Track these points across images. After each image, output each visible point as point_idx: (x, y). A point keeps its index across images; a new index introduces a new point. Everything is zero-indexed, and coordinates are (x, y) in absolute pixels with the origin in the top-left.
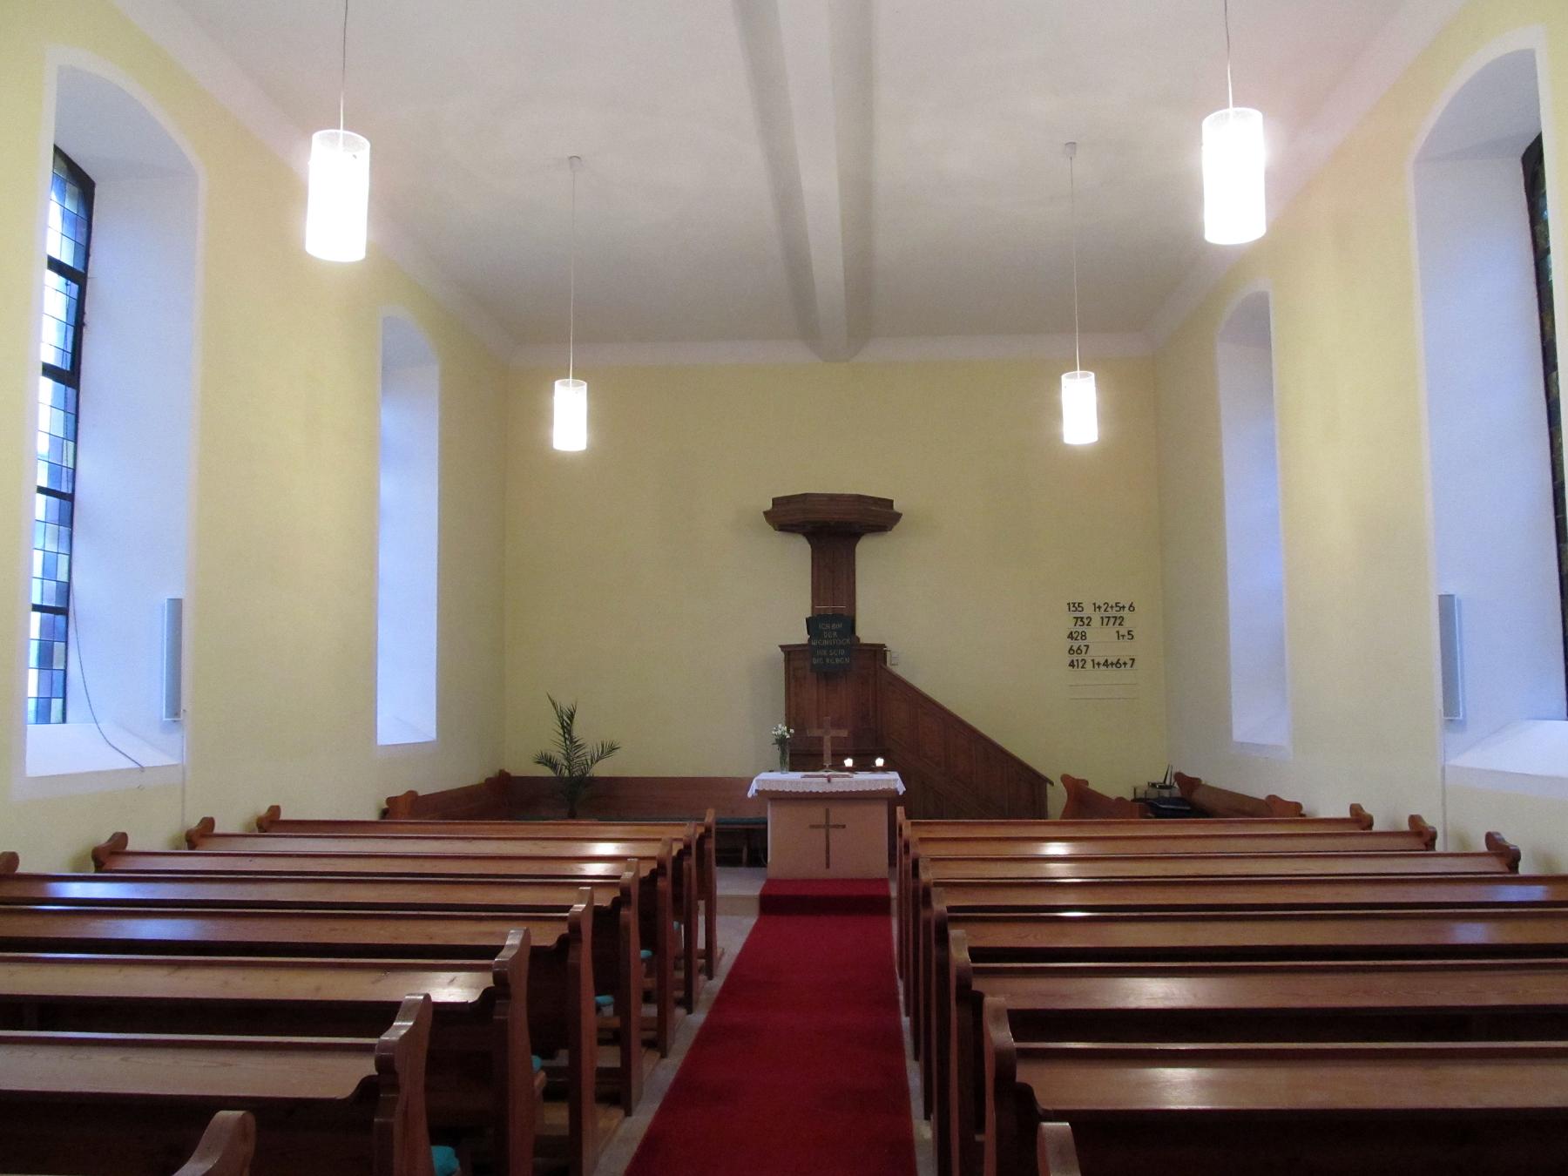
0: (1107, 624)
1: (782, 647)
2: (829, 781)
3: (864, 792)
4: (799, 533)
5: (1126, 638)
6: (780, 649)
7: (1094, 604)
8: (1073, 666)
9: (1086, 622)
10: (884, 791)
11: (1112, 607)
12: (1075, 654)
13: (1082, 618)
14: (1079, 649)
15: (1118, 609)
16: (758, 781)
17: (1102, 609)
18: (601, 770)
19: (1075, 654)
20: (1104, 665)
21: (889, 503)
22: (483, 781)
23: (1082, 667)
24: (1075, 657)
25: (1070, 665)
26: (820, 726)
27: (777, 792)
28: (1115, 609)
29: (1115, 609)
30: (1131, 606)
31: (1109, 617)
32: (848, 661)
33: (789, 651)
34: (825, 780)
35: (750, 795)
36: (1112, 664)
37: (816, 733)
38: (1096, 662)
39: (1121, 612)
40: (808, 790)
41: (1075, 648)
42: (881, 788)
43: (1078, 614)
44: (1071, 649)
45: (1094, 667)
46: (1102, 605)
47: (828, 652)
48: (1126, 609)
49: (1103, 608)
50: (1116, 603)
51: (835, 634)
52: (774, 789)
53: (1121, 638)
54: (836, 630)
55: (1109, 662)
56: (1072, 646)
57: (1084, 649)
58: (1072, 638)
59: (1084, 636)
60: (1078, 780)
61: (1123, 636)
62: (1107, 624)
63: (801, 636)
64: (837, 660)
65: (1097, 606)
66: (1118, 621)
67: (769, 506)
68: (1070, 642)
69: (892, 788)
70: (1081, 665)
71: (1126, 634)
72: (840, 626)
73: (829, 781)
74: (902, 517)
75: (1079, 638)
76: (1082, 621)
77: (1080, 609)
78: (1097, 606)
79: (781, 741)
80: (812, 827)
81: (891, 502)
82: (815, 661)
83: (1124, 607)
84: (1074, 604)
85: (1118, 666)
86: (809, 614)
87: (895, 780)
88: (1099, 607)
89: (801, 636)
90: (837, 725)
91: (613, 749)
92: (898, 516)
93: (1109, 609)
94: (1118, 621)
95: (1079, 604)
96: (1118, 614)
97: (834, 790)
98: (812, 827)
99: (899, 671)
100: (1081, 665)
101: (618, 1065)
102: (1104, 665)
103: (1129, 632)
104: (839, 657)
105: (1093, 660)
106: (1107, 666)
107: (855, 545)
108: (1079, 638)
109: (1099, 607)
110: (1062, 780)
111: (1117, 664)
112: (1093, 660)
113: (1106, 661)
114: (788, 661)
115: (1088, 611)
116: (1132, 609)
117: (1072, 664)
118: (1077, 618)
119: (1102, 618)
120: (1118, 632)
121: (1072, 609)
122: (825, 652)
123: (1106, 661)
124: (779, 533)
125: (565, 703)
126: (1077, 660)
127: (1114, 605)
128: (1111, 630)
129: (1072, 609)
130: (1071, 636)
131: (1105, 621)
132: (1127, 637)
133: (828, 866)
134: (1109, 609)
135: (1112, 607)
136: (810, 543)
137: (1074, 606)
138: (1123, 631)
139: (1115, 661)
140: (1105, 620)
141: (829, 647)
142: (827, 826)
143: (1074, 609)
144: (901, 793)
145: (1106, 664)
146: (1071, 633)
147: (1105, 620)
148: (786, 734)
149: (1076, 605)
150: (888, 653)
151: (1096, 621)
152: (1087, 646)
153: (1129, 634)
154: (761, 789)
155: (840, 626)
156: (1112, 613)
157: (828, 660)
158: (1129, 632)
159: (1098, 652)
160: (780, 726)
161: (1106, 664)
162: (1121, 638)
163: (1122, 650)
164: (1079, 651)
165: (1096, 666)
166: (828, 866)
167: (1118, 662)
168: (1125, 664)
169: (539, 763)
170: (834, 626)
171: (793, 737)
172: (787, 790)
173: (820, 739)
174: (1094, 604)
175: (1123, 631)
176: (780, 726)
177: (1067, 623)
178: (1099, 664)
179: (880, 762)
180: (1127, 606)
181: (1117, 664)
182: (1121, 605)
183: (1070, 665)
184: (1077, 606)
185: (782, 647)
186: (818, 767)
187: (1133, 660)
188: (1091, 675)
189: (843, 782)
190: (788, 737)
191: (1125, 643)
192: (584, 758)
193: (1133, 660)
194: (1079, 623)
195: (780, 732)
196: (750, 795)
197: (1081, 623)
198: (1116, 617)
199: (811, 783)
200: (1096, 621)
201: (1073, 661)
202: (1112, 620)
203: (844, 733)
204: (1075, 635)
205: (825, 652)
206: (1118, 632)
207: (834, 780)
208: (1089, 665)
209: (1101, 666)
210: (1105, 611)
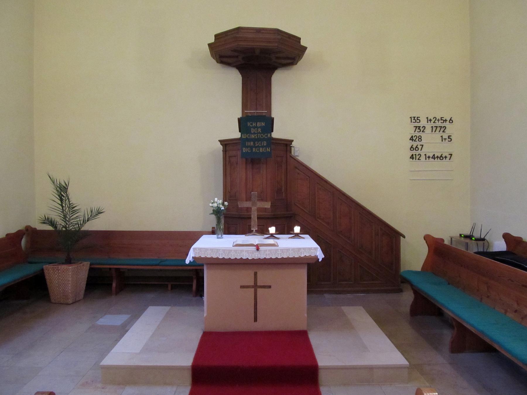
0: (435, 132)
1: (221, 141)
2: (258, 249)
3: (288, 259)
4: (234, 66)
5: (447, 141)
6: (219, 143)
7: (427, 118)
8: (413, 158)
9: (422, 130)
10: (305, 258)
11: (438, 120)
12: (414, 151)
13: (420, 127)
14: (416, 147)
15: (442, 121)
16: (194, 249)
17: (432, 122)
18: (87, 227)
19: (414, 151)
20: (432, 158)
21: (298, 39)
22: (4, 236)
23: (418, 159)
24: (414, 152)
25: (411, 158)
26: (248, 199)
27: (212, 258)
28: (440, 121)
29: (440, 121)
30: (450, 120)
31: (437, 127)
32: (269, 150)
33: (226, 144)
34: (254, 248)
35: (187, 262)
36: (438, 157)
37: (246, 204)
38: (427, 156)
39: (444, 123)
40: (238, 258)
41: (414, 147)
42: (302, 256)
43: (417, 124)
44: (412, 147)
45: (426, 159)
46: (432, 119)
47: (254, 144)
48: (448, 122)
49: (433, 120)
50: (441, 118)
51: (259, 130)
52: (209, 256)
53: (444, 140)
54: (260, 127)
55: (436, 156)
56: (413, 145)
57: (420, 147)
58: (412, 140)
59: (420, 139)
60: (437, 239)
61: (445, 139)
62: (435, 132)
63: (235, 134)
64: (261, 150)
65: (429, 119)
66: (442, 130)
67: (212, 40)
68: (411, 143)
69: (313, 255)
70: (417, 157)
71: (447, 138)
72: (263, 124)
73: (258, 249)
74: (307, 51)
75: (417, 140)
76: (419, 129)
77: (418, 121)
78: (429, 119)
79: (217, 212)
80: (242, 287)
81: (300, 39)
82: (244, 150)
83: (446, 120)
84: (414, 117)
85: (441, 158)
86: (240, 115)
87: (315, 249)
88: (430, 120)
89: (235, 134)
90: (261, 199)
91: (99, 213)
92: (306, 48)
93: (436, 121)
94: (442, 130)
95: (417, 117)
96: (443, 125)
97: (262, 257)
98: (242, 287)
99: (302, 158)
100: (417, 157)
101: (225, 202)
102: (432, 158)
103: (449, 137)
104: (263, 147)
105: (425, 155)
106: (434, 158)
107: (271, 76)
108: (417, 140)
109: (430, 120)
110: (425, 239)
111: (441, 157)
112: (425, 155)
113: (434, 155)
114: (225, 151)
115: (423, 122)
116: (451, 121)
117: (412, 157)
118: (416, 127)
119: (432, 127)
120: (442, 136)
121: (413, 121)
122: (252, 143)
123: (434, 155)
124: (219, 65)
125: (61, 179)
126: (416, 155)
127: (440, 119)
128: (437, 136)
129: (413, 121)
130: (412, 139)
131: (434, 129)
132: (448, 140)
133: (256, 320)
134: (436, 121)
135: (438, 120)
136: (241, 73)
137: (414, 119)
138: (445, 136)
139: (439, 156)
140: (434, 129)
141: (254, 140)
142: (256, 286)
143: (414, 121)
144: (320, 260)
145: (434, 157)
146: (412, 137)
147: (434, 129)
148: (221, 206)
149: (416, 118)
150: (293, 148)
151: (428, 130)
152: (422, 145)
153: (449, 138)
154: (197, 256)
155: (263, 124)
156: (439, 124)
157: (254, 150)
158: (449, 137)
159: (428, 150)
160: (216, 199)
161: (434, 157)
162: (444, 140)
163: (444, 149)
164: (417, 149)
165: (427, 159)
166: (256, 320)
167: (441, 156)
168: (446, 157)
169: (44, 223)
170: (258, 124)
171: (227, 209)
172: (221, 257)
173: (248, 209)
174: (427, 118)
175: (445, 136)
176: (216, 199)
177: (410, 131)
178: (429, 157)
179: (297, 229)
180: (448, 119)
181: (441, 157)
182: (444, 119)
183: (411, 158)
184: (416, 119)
185: (221, 141)
186: (246, 231)
187: (451, 155)
188: (423, 165)
189: (269, 250)
190: (223, 208)
191: (446, 143)
192: (78, 219)
193: (451, 155)
194: (417, 130)
195: (215, 205)
196: (187, 262)
197: (419, 131)
198: (441, 127)
199: (242, 251)
200: (428, 130)
201: (413, 155)
202: (438, 129)
203: (267, 205)
204: (414, 138)
205: (252, 143)
206: (442, 136)
207: (261, 248)
208: (423, 158)
209: (430, 158)
210: (434, 122)
